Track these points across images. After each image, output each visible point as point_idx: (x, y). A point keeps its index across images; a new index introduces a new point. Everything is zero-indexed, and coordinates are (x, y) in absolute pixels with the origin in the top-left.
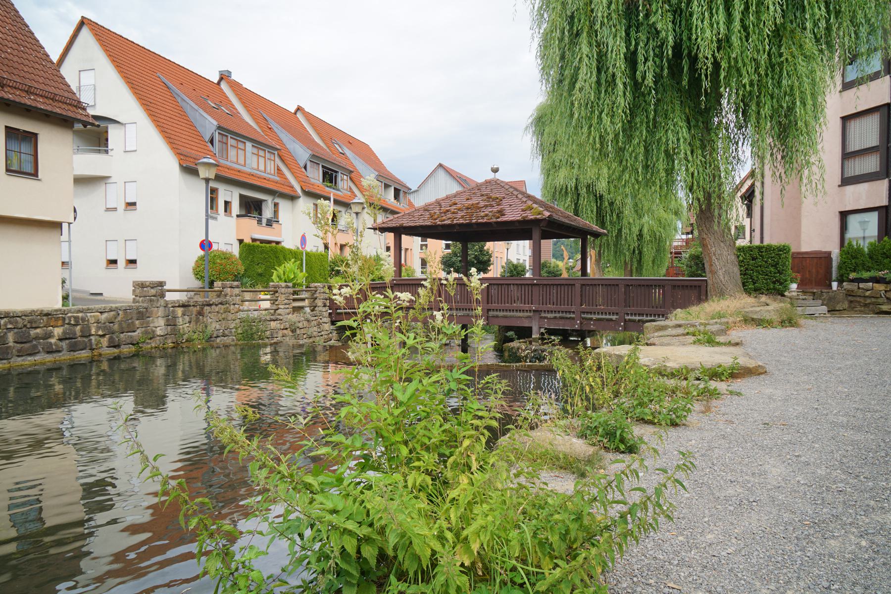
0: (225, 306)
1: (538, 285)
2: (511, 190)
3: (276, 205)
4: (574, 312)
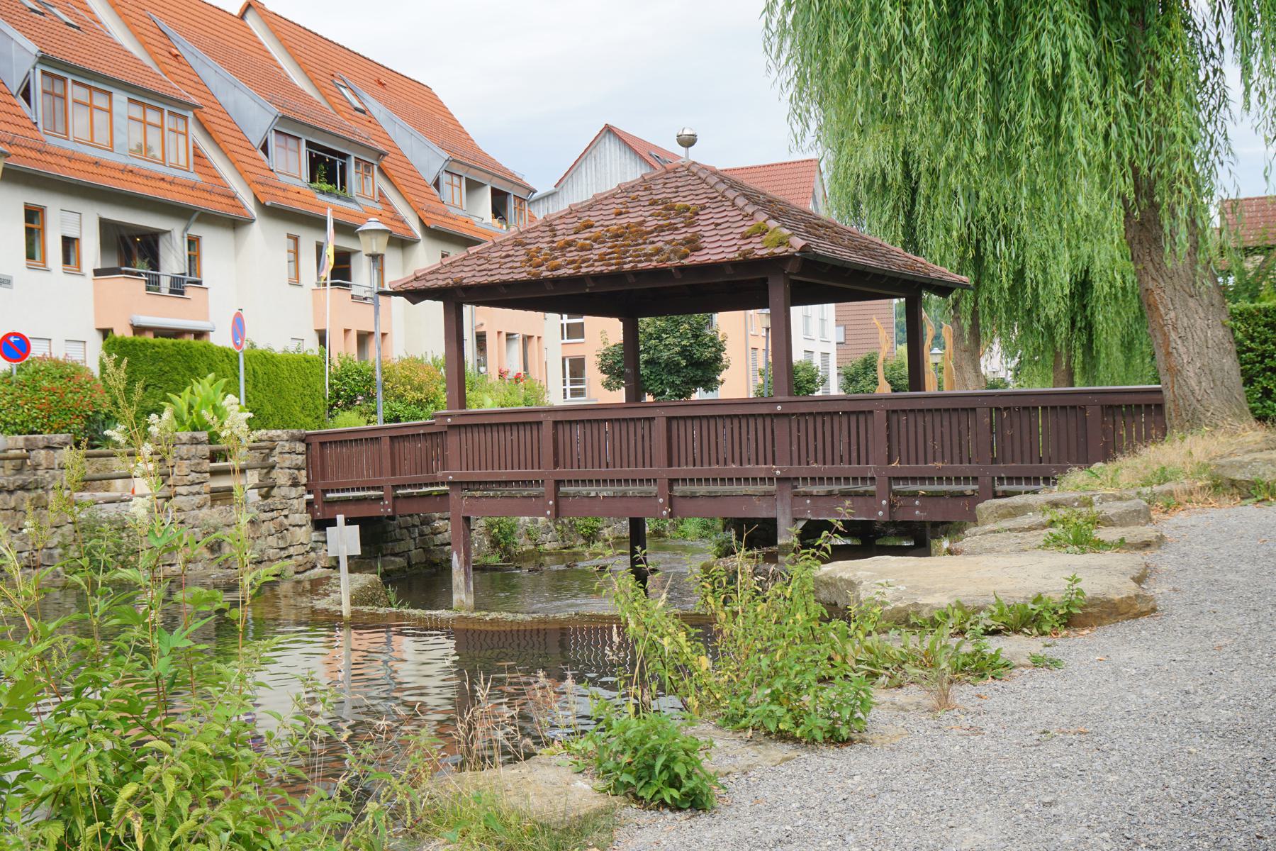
0: (33, 494)
1: (787, 415)
2: (722, 187)
3: (193, 243)
4: (872, 479)
